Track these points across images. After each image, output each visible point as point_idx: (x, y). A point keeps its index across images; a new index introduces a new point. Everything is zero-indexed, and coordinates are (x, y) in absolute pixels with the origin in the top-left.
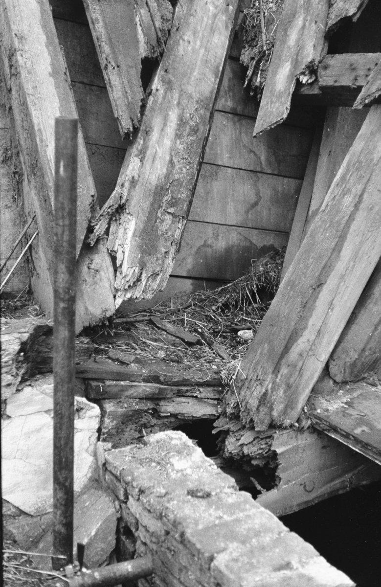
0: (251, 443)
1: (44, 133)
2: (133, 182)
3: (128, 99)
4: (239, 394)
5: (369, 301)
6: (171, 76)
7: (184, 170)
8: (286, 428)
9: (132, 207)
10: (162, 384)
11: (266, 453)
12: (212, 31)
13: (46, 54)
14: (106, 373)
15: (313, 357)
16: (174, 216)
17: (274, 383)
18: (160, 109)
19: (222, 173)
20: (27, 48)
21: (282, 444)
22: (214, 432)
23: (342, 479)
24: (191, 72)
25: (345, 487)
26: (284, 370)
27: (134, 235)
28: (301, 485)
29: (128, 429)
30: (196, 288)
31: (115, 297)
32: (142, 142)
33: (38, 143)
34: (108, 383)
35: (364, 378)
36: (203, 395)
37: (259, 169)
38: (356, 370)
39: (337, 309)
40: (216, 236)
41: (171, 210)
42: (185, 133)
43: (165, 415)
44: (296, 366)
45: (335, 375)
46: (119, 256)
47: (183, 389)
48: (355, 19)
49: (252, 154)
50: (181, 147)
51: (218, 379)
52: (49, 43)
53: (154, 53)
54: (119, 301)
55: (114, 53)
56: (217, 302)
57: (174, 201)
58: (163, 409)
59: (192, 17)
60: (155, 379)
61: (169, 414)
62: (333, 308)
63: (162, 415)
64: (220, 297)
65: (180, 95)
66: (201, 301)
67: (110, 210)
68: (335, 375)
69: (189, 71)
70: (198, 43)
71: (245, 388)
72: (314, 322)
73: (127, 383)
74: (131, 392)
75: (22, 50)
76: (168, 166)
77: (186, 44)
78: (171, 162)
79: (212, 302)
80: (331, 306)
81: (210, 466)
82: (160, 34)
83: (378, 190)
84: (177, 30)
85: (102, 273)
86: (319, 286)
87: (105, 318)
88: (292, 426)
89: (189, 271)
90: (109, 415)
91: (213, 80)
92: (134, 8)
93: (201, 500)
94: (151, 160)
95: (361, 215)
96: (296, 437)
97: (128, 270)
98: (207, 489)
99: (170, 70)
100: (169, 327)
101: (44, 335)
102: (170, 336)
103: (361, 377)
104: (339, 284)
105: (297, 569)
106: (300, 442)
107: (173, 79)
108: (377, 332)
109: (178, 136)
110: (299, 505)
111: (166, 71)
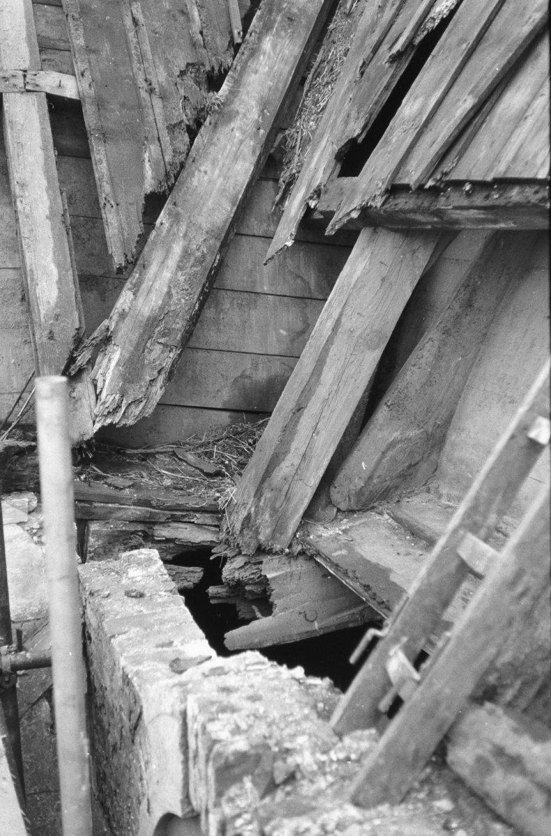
0: (241, 567)
1: (35, 273)
2: (123, 315)
3: (123, 235)
4: (230, 519)
5: (372, 426)
6: (179, 209)
7: (183, 301)
8: (276, 553)
9: (119, 338)
10: (154, 508)
11: (258, 578)
12: (236, 158)
13: (46, 198)
14: (95, 495)
15: (300, 482)
16: (165, 345)
17: (256, 507)
18: (163, 242)
19: (261, 301)
20: (27, 194)
21: (273, 570)
22: (211, 558)
23: (352, 611)
24: (204, 203)
25: (356, 620)
26: (268, 494)
27: (118, 364)
28: (300, 613)
29: (116, 550)
30: (234, 421)
31: (94, 422)
32: (137, 275)
33: (29, 282)
34: (96, 504)
35: (373, 508)
36: (200, 521)
37: (306, 295)
38: (363, 499)
39: (323, 434)
40: (255, 366)
41: (162, 340)
42: (188, 265)
43: (159, 539)
44: (281, 490)
45: (339, 503)
46: (99, 385)
47: (178, 515)
48: (360, 140)
49: (299, 281)
50: (182, 278)
51: (215, 505)
52: (50, 187)
53: (161, 187)
54: (98, 426)
55: (114, 191)
56: (254, 435)
57: (166, 331)
58: (156, 533)
59: (213, 146)
60: (146, 503)
61: (164, 539)
62: (318, 433)
63: (156, 538)
64: (259, 430)
65: (188, 227)
66: (237, 433)
67: (93, 342)
68: (339, 503)
69: (201, 202)
70: (217, 172)
71: (234, 514)
72: (298, 445)
73: (117, 505)
74: (119, 514)
75: (22, 197)
76: (165, 298)
77: (202, 174)
78: (169, 294)
79: (249, 435)
80: (315, 430)
81: (162, 575)
82: (168, 167)
83: (358, 314)
84: (193, 161)
85: (84, 401)
86: (299, 410)
87: (82, 441)
88: (282, 551)
89: (224, 403)
90: (92, 534)
91: (229, 208)
92: (144, 144)
93: (134, 599)
94: (145, 293)
95: (341, 338)
96: (289, 563)
97: (107, 396)
98: (139, 589)
99: (180, 203)
100: (191, 457)
101: (17, 454)
102: (189, 467)
103: (370, 506)
104: (322, 408)
105: (176, 646)
106: (294, 568)
107: (182, 211)
108: (386, 459)
109: (180, 268)
110: (299, 634)
111: (175, 204)
